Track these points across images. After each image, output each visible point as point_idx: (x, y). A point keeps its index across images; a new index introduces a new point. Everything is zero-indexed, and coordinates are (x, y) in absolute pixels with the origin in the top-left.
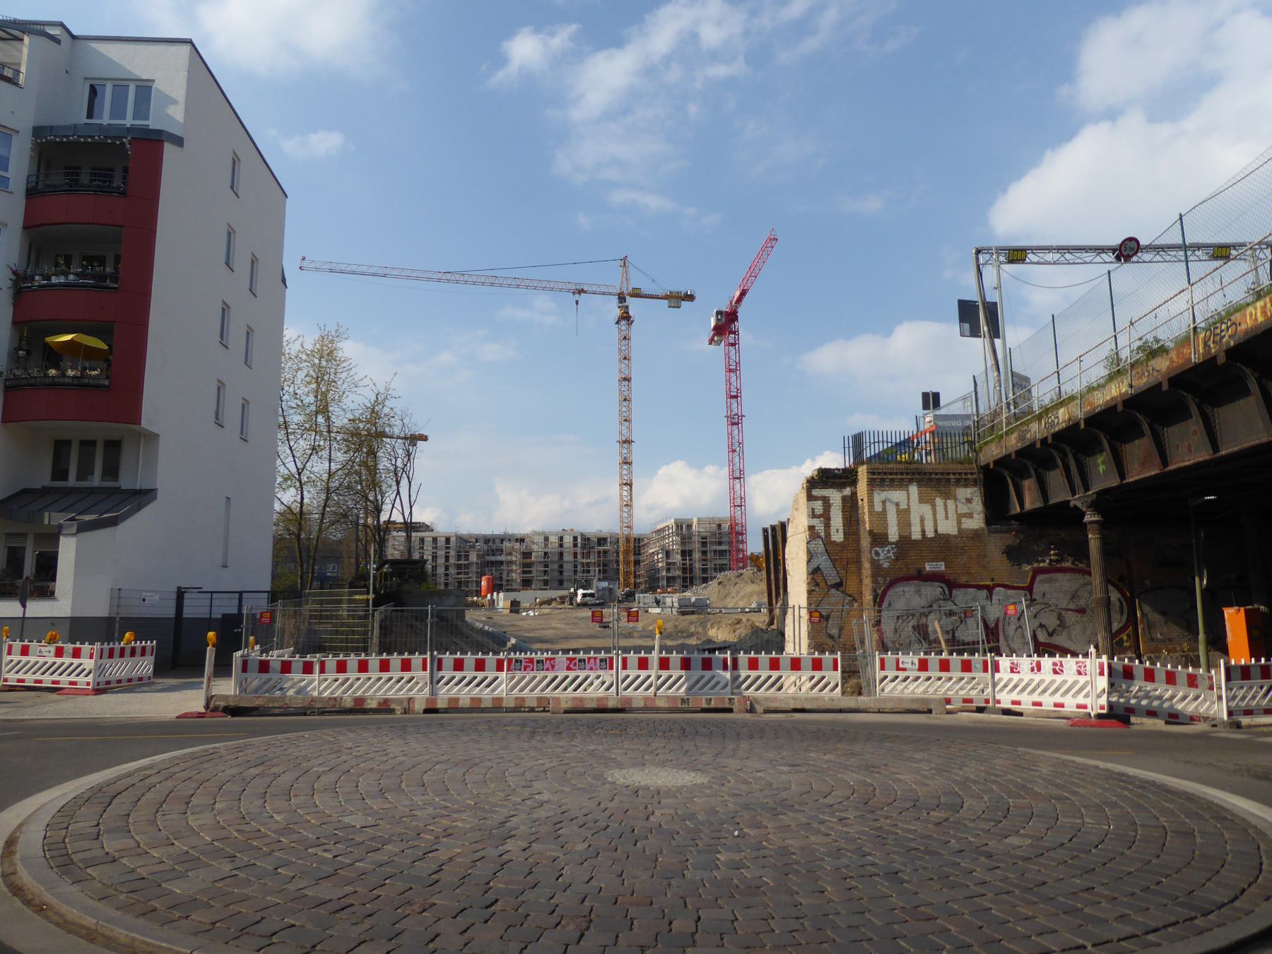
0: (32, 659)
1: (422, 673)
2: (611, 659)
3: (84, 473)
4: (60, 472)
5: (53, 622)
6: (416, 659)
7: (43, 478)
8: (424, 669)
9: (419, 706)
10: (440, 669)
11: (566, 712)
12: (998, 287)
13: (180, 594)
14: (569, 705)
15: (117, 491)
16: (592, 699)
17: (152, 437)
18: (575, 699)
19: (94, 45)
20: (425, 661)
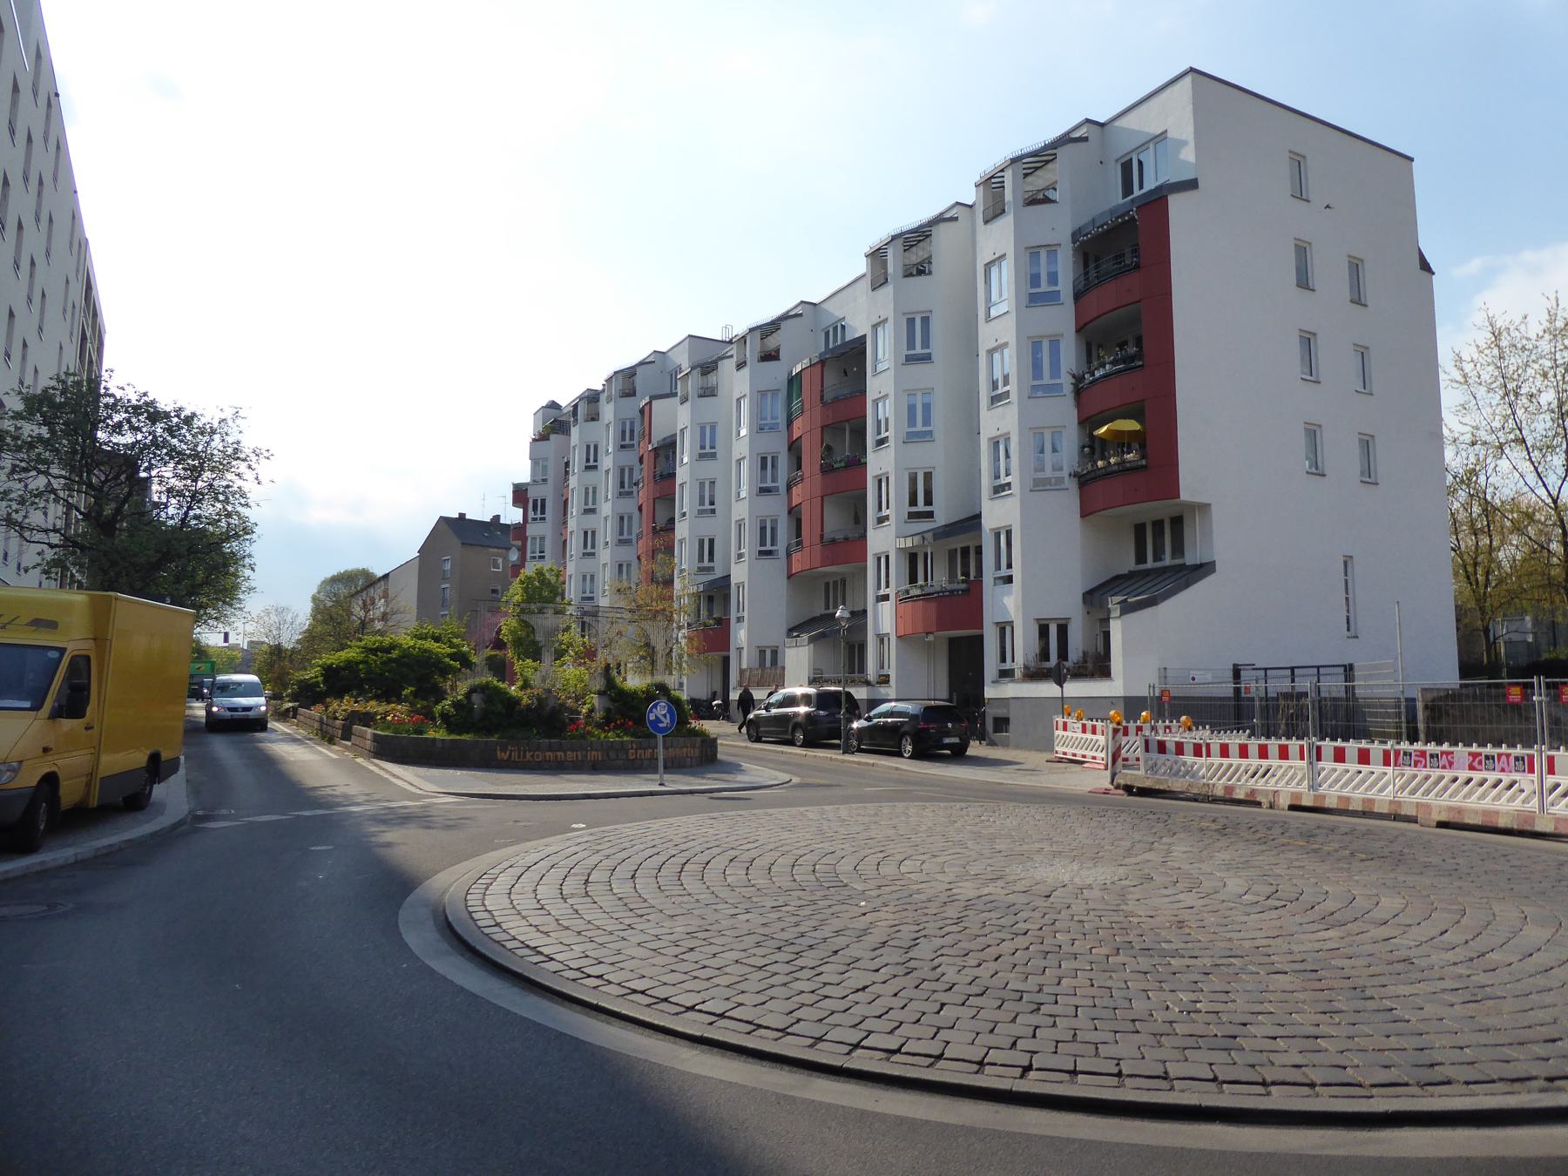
0: (1069, 734)
1: (1300, 763)
2: (1531, 758)
3: (1157, 558)
4: (1141, 558)
5: (1112, 701)
6: (1294, 744)
7: (1128, 563)
8: (1302, 758)
9: (1284, 801)
10: (1319, 759)
11: (1442, 825)
12: (7, 539)
13: (1236, 673)
14: (1444, 817)
15: (1183, 567)
16: (1476, 812)
17: (1204, 508)
18: (1451, 809)
19: (1117, 123)
20: (1302, 747)
